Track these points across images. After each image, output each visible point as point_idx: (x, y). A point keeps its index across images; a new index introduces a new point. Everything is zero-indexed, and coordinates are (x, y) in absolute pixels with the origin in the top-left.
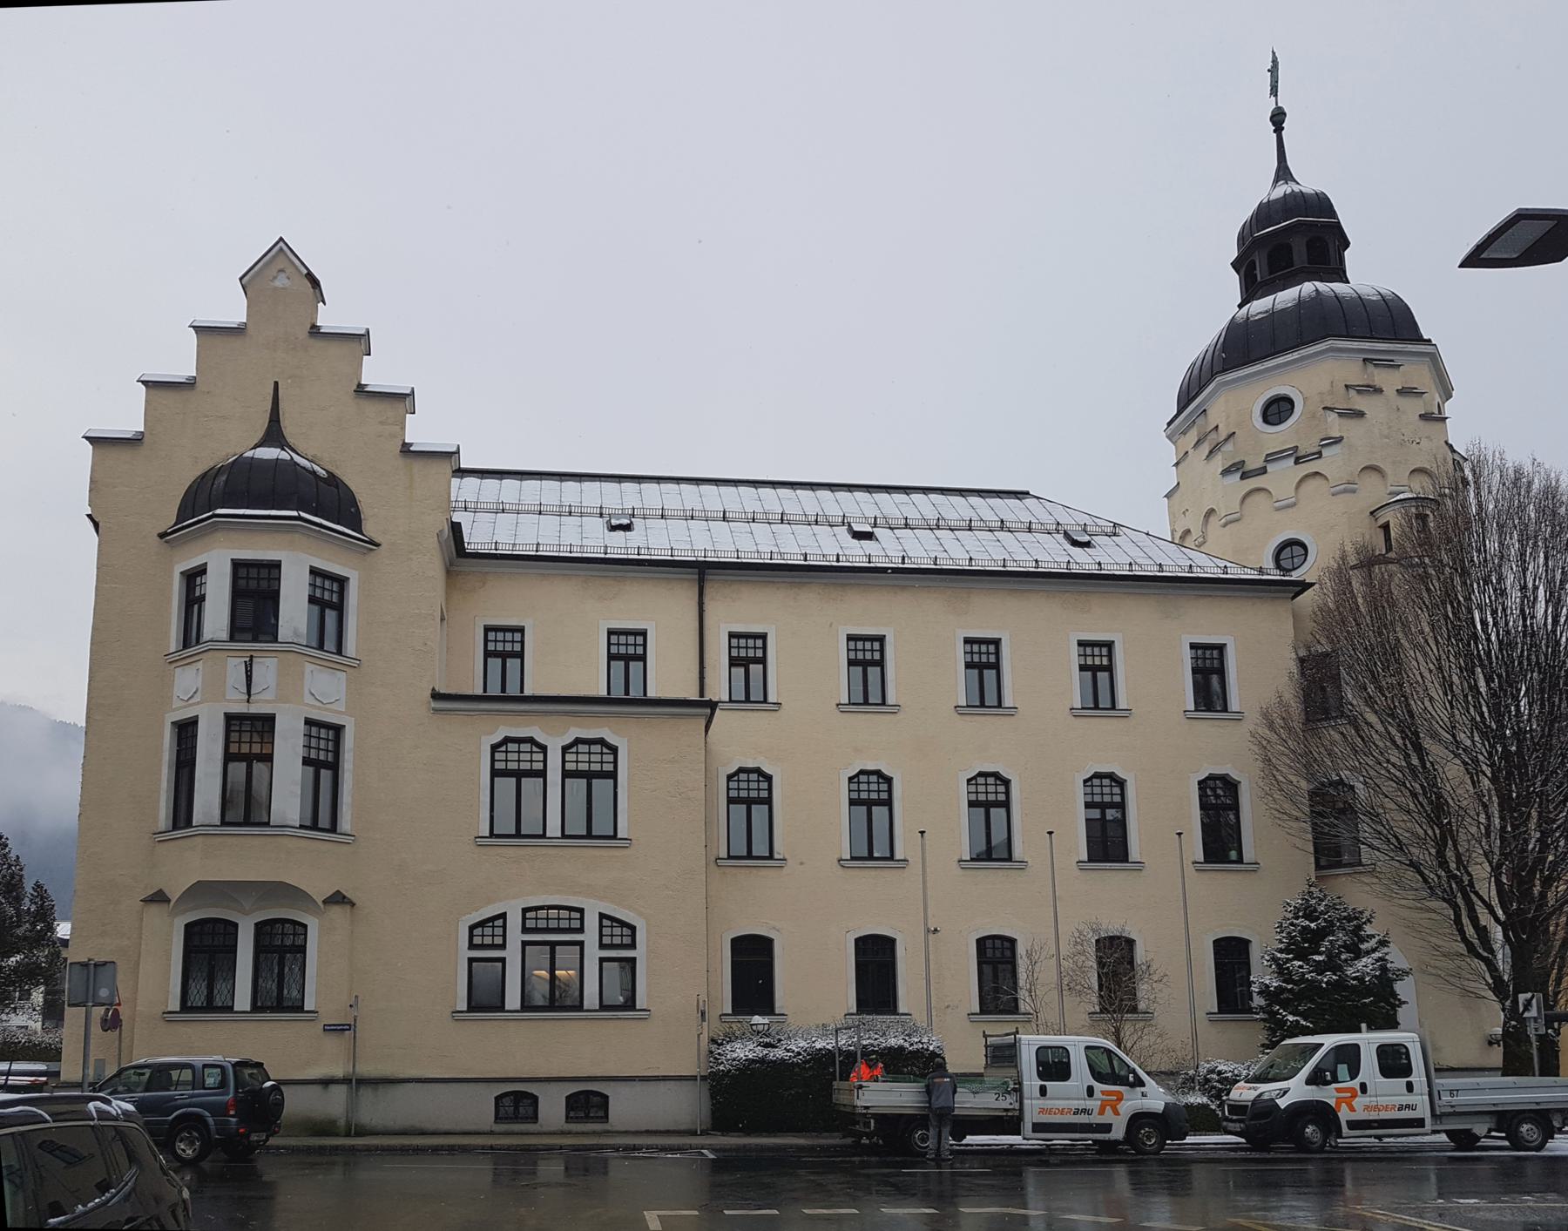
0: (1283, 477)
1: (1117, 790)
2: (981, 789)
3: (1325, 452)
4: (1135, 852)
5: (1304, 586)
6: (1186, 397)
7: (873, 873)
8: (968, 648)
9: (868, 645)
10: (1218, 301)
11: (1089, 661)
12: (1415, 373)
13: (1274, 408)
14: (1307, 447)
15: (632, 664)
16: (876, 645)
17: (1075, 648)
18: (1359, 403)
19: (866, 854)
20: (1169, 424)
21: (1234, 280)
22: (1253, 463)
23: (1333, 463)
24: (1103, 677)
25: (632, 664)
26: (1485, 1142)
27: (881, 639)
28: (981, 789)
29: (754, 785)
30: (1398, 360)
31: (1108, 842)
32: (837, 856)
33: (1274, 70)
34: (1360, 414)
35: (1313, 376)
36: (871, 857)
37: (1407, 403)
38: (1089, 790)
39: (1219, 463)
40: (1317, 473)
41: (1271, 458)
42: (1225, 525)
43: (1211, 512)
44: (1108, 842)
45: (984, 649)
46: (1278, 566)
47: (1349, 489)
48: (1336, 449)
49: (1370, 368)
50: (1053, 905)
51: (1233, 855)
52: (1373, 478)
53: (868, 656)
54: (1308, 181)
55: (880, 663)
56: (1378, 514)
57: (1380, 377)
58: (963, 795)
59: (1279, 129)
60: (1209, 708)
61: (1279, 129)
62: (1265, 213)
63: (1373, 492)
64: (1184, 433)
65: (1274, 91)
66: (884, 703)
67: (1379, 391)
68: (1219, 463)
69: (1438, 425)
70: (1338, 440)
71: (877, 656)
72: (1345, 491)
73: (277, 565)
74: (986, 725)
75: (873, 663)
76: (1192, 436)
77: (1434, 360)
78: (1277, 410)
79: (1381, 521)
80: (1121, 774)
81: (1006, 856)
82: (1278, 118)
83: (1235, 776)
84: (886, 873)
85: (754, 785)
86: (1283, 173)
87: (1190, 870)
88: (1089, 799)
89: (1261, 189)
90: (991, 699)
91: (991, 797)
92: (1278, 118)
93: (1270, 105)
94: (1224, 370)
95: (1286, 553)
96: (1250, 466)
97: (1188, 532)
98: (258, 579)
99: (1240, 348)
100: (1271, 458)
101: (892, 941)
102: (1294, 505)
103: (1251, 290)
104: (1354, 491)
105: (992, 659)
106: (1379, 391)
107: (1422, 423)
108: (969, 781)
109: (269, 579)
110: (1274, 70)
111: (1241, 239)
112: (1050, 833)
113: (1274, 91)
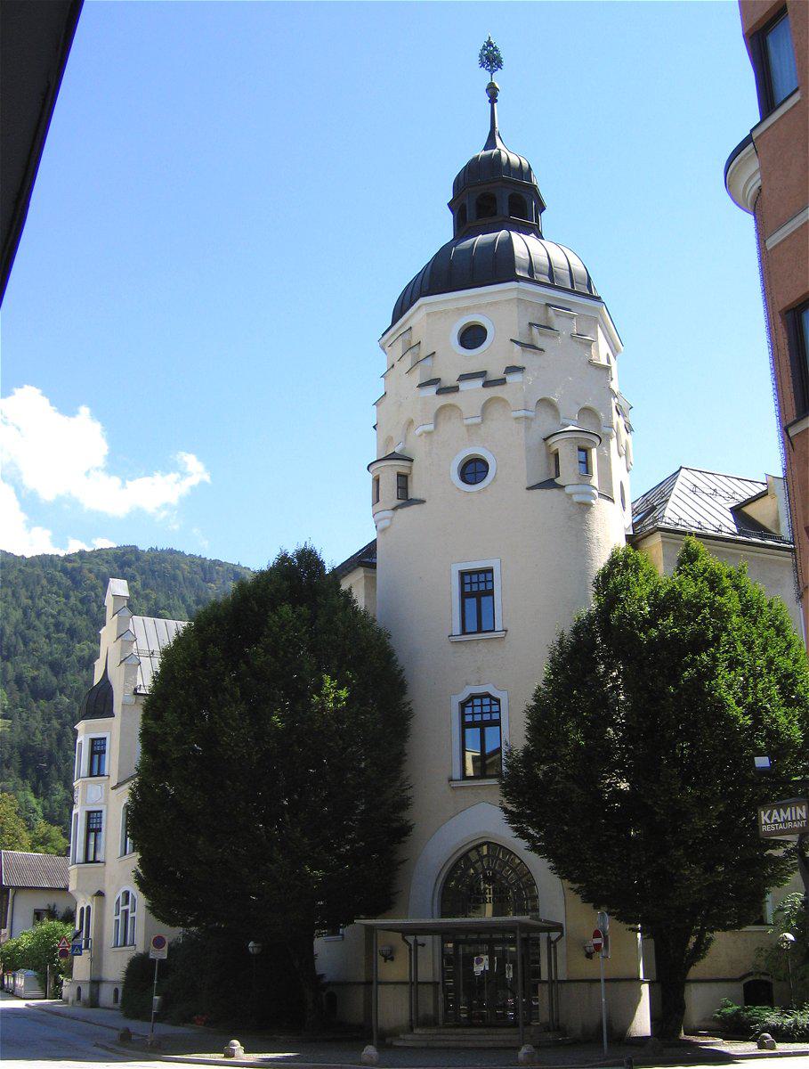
6: (401, 309)
10: (435, 230)
15: (487, 729)
21: (449, 218)
22: (449, 379)
25: (487, 729)
26: (77, 928)
54: (510, 153)
59: (493, 100)
61: (493, 100)
68: (417, 377)
70: (519, 369)
73: (111, 715)
86: (491, 143)
93: (499, 79)
96: (479, 383)
98: (478, 583)
99: (442, 276)
103: (463, 227)
109: (486, 582)
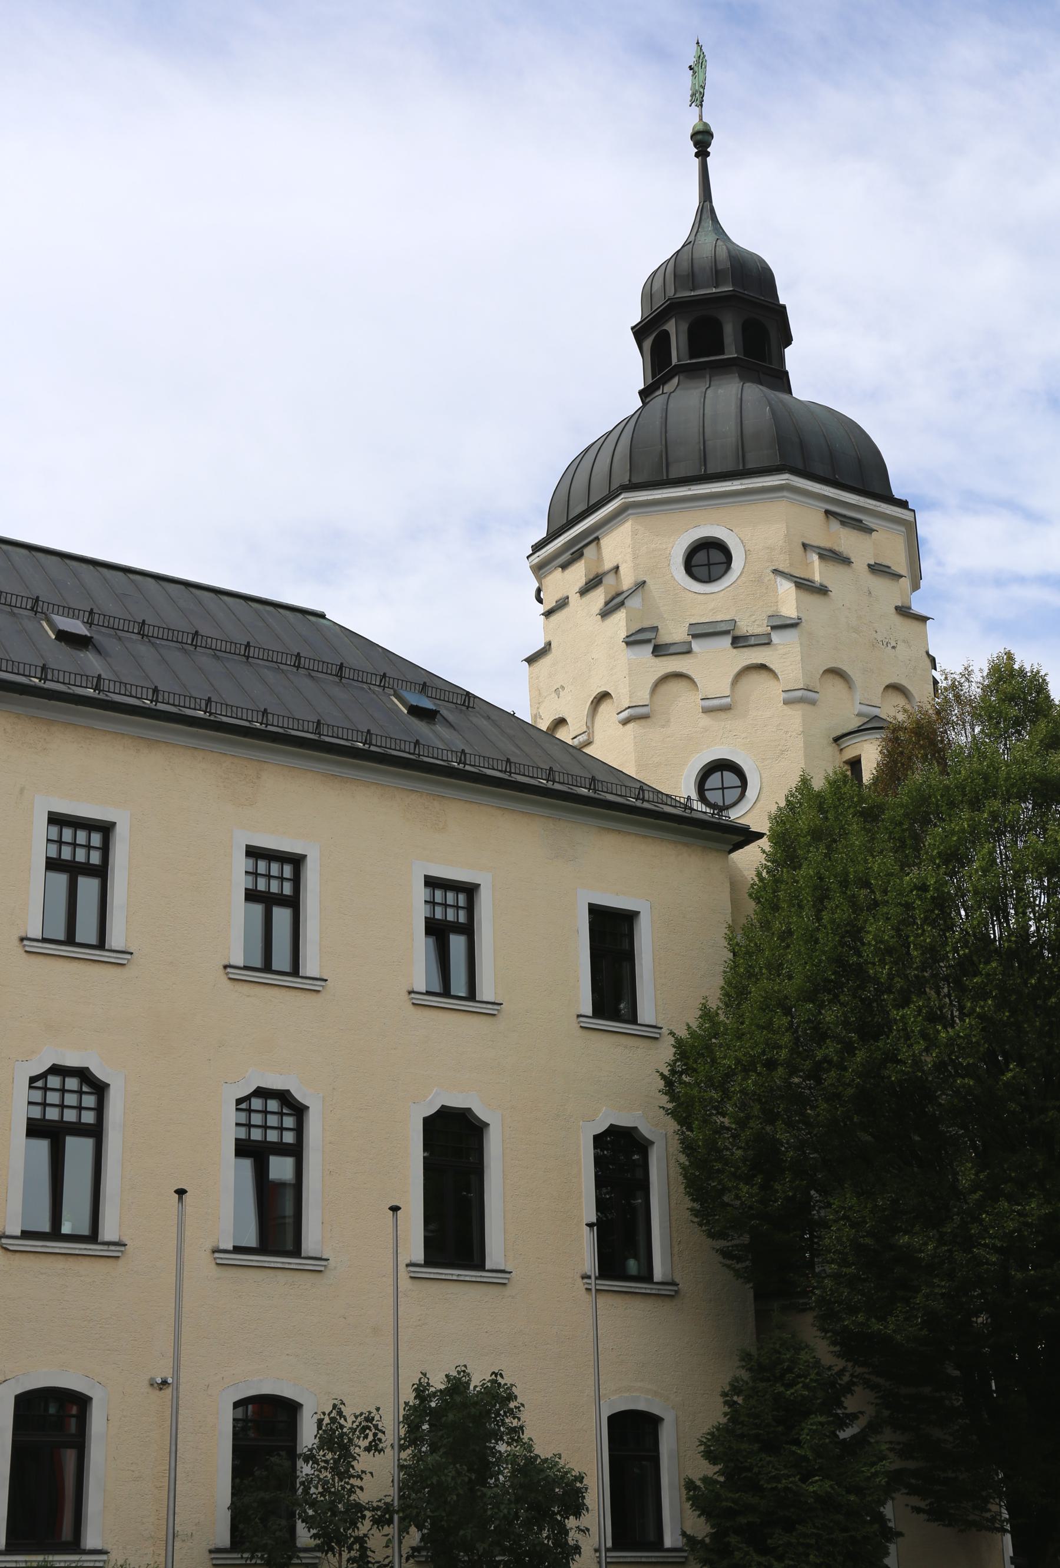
0: (714, 666)
1: (89, 1101)
2: (53, 1098)
3: (776, 637)
4: (495, 1252)
5: (746, 836)
7: (60, 1264)
8: (54, 830)
9: (82, 837)
11: (66, 854)
12: (886, 544)
13: (701, 557)
14: (751, 624)
16: (96, 839)
17: (40, 828)
18: (817, 571)
19: (46, 1228)
20: (537, 547)
23: (787, 657)
24: (88, 886)
27: (106, 829)
28: (53, 1098)
29: (71, 1099)
30: (868, 521)
31: (454, 1232)
32: (209, 1245)
33: (698, 67)
34: (822, 591)
35: (766, 526)
36: (55, 1234)
37: (880, 585)
38: (37, 1096)
39: (619, 624)
40: (763, 667)
41: (703, 632)
42: (625, 722)
43: (604, 696)
44: (454, 1232)
45: (275, 869)
46: (703, 798)
47: (802, 698)
48: (791, 635)
49: (835, 525)
50: (359, 1338)
51: (632, 1266)
52: (834, 689)
53: (81, 856)
54: (745, 230)
55: (101, 872)
56: (845, 742)
57: (846, 540)
58: (227, 1131)
59: (702, 153)
60: (615, 1016)
61: (702, 153)
62: (681, 269)
63: (843, 709)
64: (564, 567)
65: (698, 98)
66: (101, 945)
67: (846, 561)
69: (915, 625)
71: (95, 858)
72: (801, 700)
74: (270, 1004)
75: (88, 870)
76: (578, 574)
77: (911, 528)
78: (707, 559)
79: (849, 754)
80: (99, 1072)
81: (85, 1230)
82: (702, 140)
83: (481, 1113)
84: (84, 1267)
85: (71, 1099)
87: (199, 1261)
88: (36, 1113)
89: (667, 235)
90: (87, 931)
91: (272, 1137)
92: (702, 140)
93: (690, 121)
94: (632, 487)
95: (714, 780)
97: (561, 722)
100: (703, 632)
101: (82, 1401)
102: (726, 709)
103: (660, 370)
104: (813, 703)
105: (95, 858)
106: (846, 561)
107: (897, 620)
108: (33, 1080)
110: (698, 67)
111: (648, 295)
112: (181, 1192)
113: (698, 98)
